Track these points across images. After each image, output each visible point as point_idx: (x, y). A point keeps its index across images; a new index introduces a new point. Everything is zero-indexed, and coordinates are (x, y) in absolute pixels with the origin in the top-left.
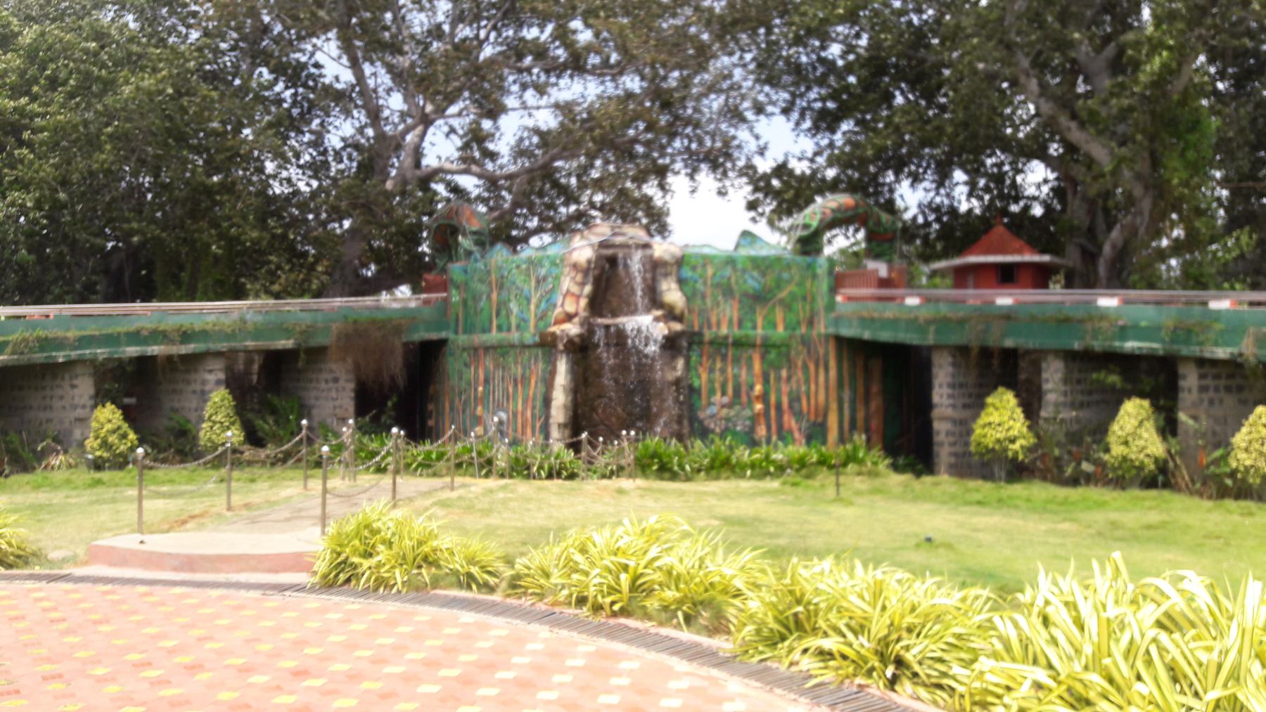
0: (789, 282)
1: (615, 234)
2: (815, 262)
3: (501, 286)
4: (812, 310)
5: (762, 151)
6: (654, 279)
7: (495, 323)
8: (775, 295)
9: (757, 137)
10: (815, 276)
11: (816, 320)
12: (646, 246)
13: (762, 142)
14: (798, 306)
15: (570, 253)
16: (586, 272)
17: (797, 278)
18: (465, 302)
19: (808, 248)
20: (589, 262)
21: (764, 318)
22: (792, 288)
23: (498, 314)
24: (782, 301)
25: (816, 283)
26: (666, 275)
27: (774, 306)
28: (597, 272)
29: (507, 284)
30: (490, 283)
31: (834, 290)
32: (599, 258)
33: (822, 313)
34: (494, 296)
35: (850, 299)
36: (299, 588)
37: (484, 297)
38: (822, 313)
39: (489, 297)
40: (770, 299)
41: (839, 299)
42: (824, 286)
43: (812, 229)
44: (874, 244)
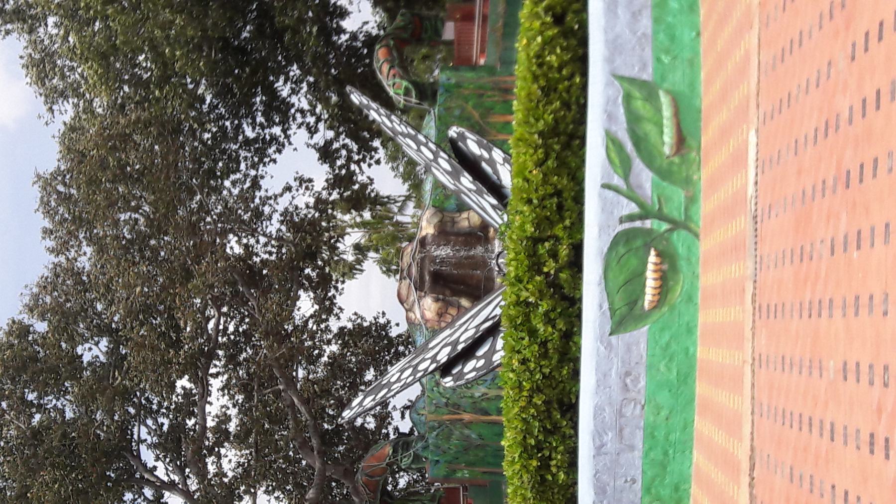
0: (463, 110)
1: (409, 275)
2: (444, 86)
3: (457, 407)
4: (493, 89)
5: (304, 182)
6: (458, 234)
7: (494, 418)
8: (477, 122)
9: (288, 189)
10: (458, 85)
11: (503, 86)
12: (423, 242)
13: (294, 184)
14: (488, 102)
15: (427, 321)
16: (447, 304)
17: (460, 102)
18: (470, 465)
19: (429, 92)
20: (437, 300)
21: (499, 132)
22: (470, 106)
23: (487, 413)
24: (483, 116)
25: (466, 85)
26: (454, 222)
27: (488, 123)
28: (448, 292)
29: (454, 399)
30: (453, 422)
31: (474, 67)
32: (433, 290)
33: (496, 78)
34: (466, 417)
35: (482, 51)
36: (742, 399)
37: (467, 432)
38: (496, 78)
39: (468, 425)
40: (480, 125)
41: (482, 62)
42: (469, 75)
43: (410, 86)
44: (424, 36)
